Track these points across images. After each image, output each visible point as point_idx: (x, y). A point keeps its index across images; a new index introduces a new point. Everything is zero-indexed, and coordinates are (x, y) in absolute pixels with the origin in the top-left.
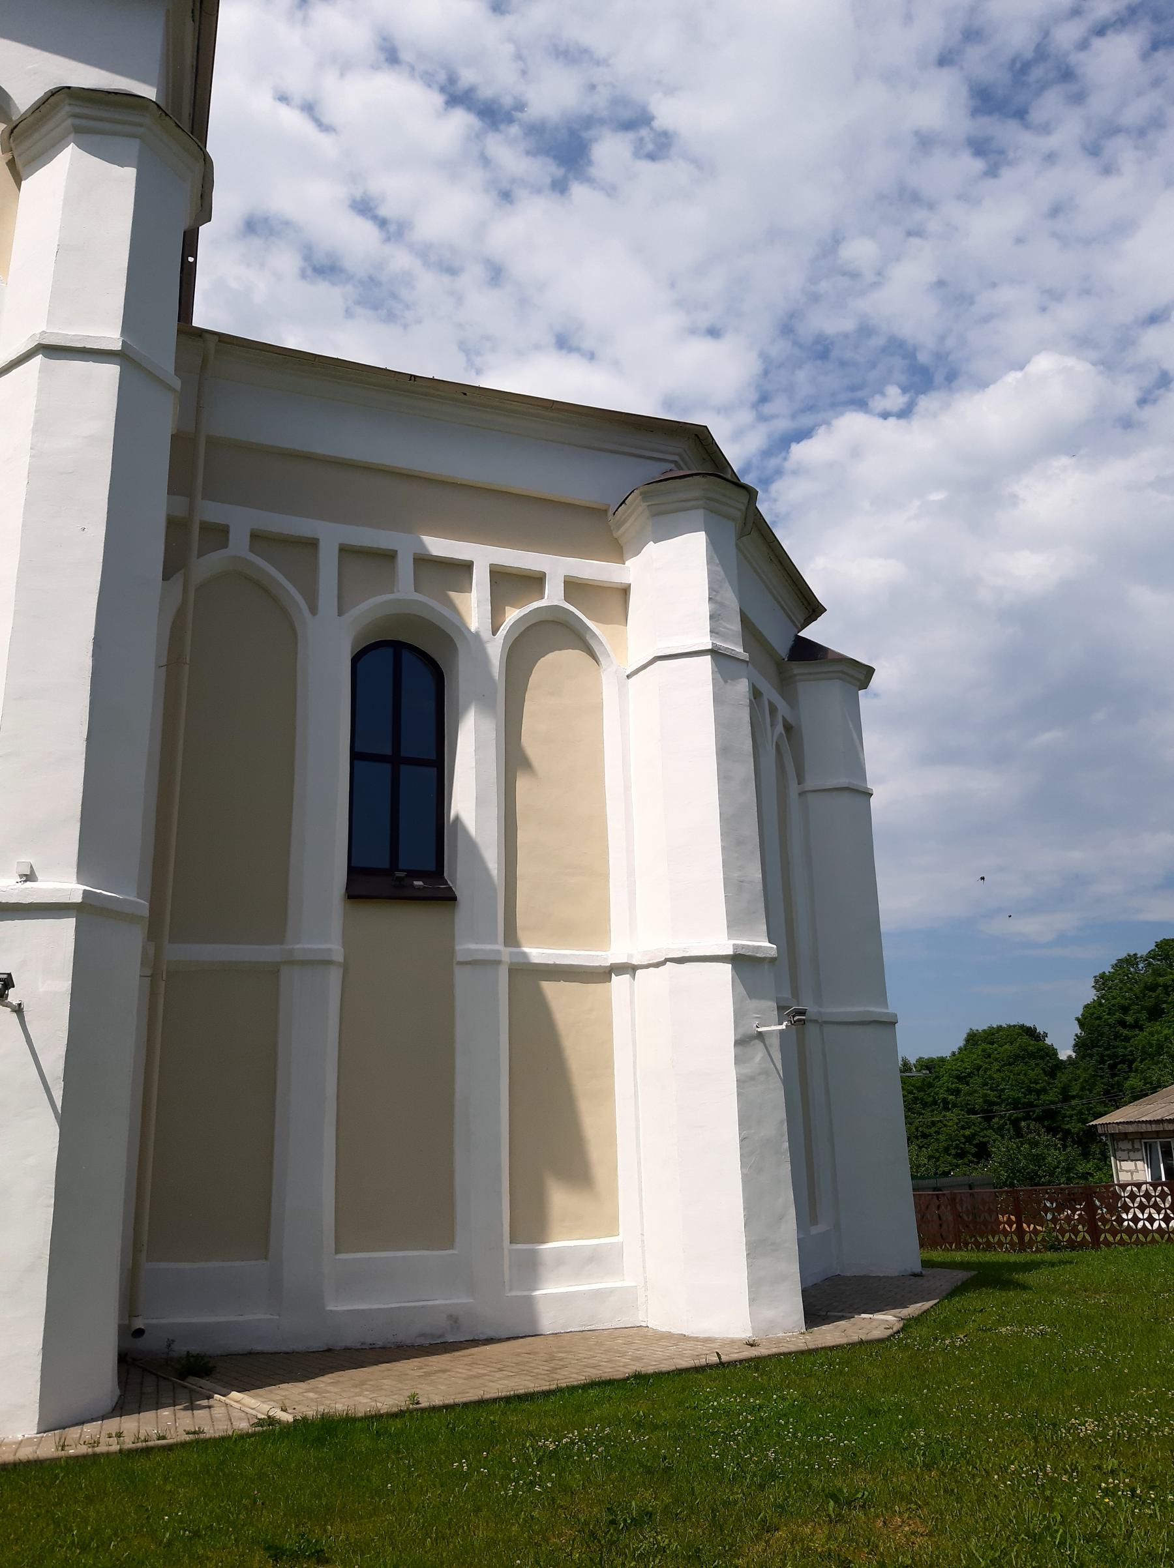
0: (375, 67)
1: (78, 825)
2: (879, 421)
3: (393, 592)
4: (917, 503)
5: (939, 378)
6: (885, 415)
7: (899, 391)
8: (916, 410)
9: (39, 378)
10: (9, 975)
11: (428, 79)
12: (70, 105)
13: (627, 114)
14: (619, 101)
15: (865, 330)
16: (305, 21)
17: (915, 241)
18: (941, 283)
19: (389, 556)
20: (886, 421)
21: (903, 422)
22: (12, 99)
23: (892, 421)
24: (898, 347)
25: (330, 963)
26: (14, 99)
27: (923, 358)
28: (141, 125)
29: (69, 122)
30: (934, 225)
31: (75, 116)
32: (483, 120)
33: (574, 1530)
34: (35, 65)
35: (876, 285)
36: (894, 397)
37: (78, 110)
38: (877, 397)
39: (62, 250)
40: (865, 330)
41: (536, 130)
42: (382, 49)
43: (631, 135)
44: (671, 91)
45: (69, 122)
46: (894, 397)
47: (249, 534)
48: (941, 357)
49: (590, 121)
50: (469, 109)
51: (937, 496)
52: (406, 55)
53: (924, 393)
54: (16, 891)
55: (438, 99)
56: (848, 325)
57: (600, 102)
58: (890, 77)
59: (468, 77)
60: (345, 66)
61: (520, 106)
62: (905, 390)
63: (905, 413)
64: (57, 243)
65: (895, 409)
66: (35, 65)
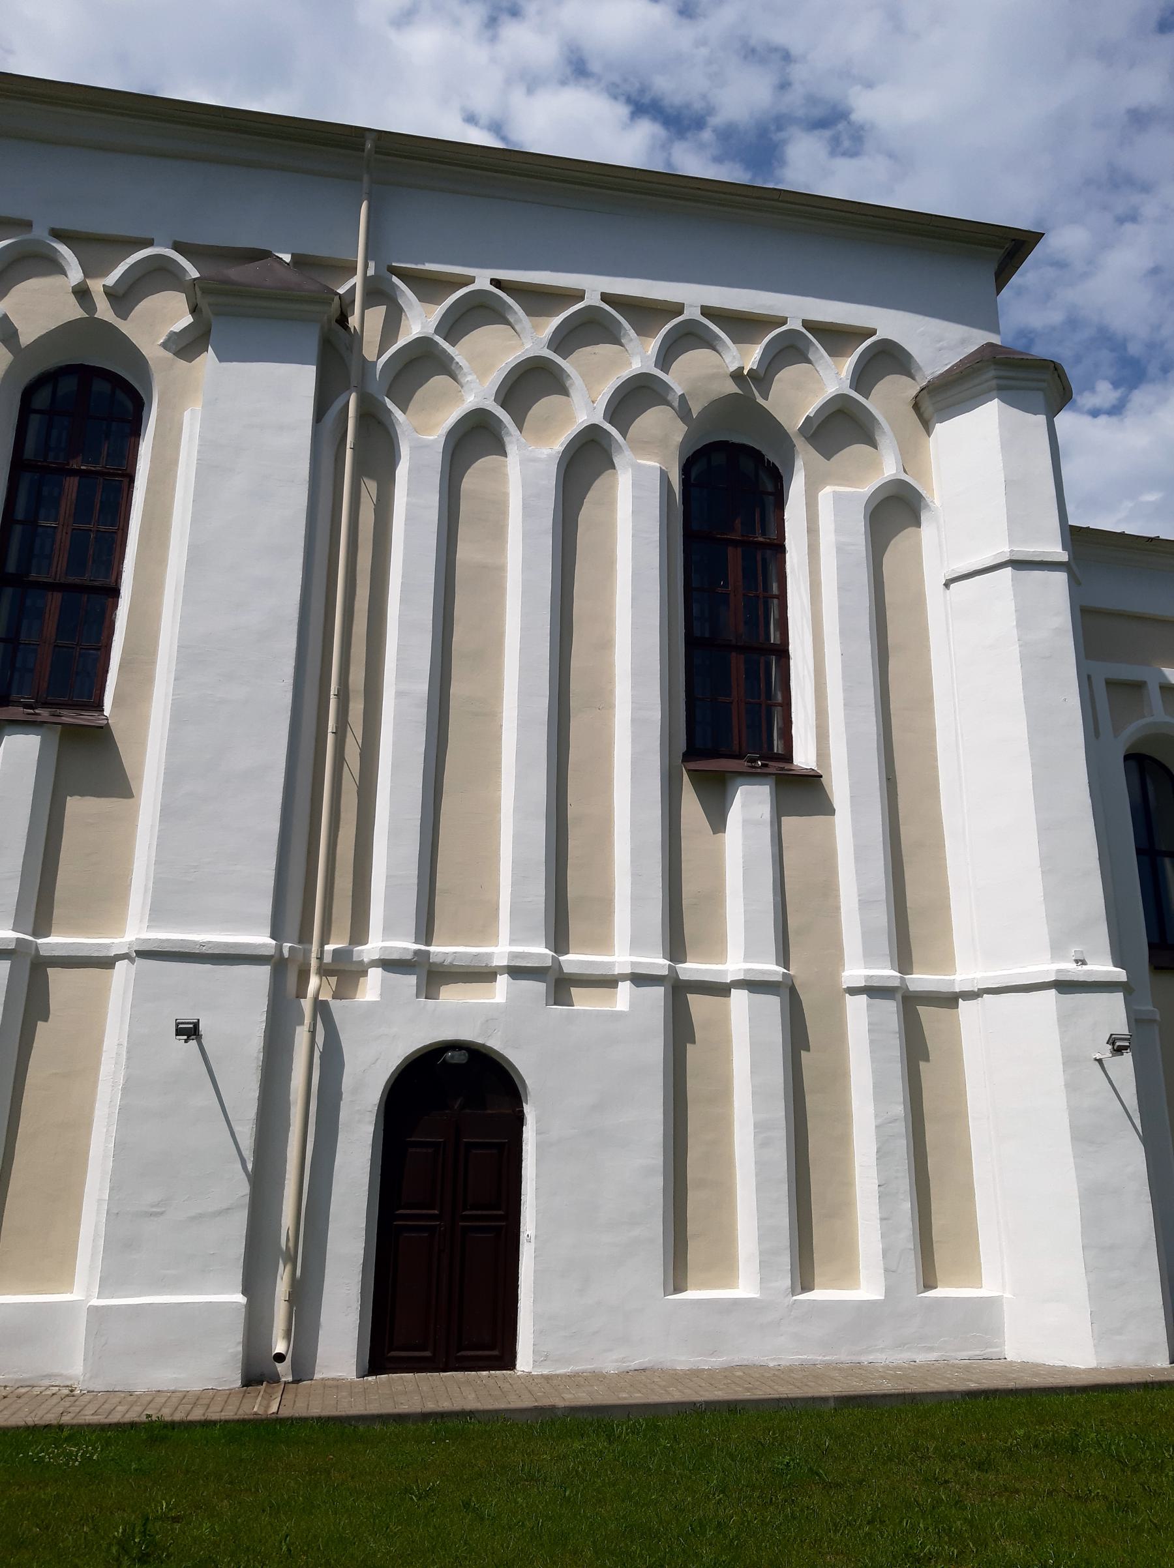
0: (563, 83)
1: (1106, 923)
2: (1087, 420)
3: (1144, 717)
4: (1129, 504)
5: (1153, 369)
6: (1095, 413)
7: (1110, 386)
8: (1129, 406)
9: (1013, 585)
10: (199, 1020)
11: (614, 92)
12: (995, 370)
13: (818, 112)
14: (812, 100)
15: (1073, 322)
16: (494, 39)
17: (1129, 227)
18: (1155, 271)
19: (1138, 686)
20: (1096, 419)
21: (1114, 419)
22: (913, 357)
23: (1103, 420)
24: (1107, 339)
25: (1155, 1021)
26: (914, 356)
27: (1134, 349)
28: (1044, 381)
29: (994, 383)
30: (1150, 208)
31: (998, 378)
32: (668, 129)
33: (1078, 1560)
34: (922, 329)
35: (1085, 276)
36: (1105, 393)
37: (1002, 373)
38: (1087, 394)
39: (1009, 484)
40: (1073, 322)
41: (727, 134)
42: (570, 62)
43: (827, 133)
44: (869, 85)
45: (994, 383)
46: (1105, 393)
47: (1104, 683)
48: (1152, 346)
49: (781, 121)
50: (654, 119)
51: (1152, 497)
52: (595, 66)
53: (1136, 388)
54: (1082, 972)
55: (622, 110)
56: (1055, 317)
57: (794, 100)
58: (1106, 53)
59: (664, 85)
60: (532, 82)
61: (711, 111)
62: (1116, 385)
63: (1116, 410)
64: (1003, 480)
65: (1107, 405)
66: (922, 329)
